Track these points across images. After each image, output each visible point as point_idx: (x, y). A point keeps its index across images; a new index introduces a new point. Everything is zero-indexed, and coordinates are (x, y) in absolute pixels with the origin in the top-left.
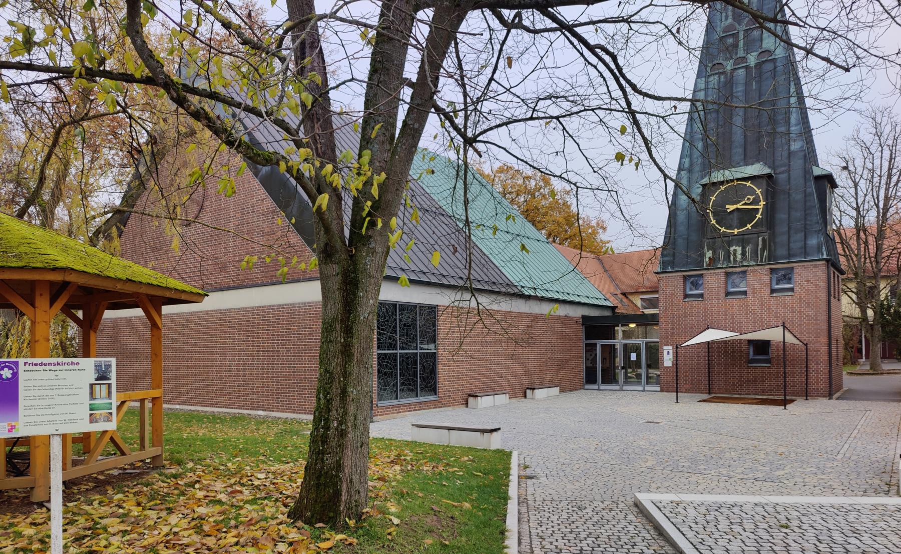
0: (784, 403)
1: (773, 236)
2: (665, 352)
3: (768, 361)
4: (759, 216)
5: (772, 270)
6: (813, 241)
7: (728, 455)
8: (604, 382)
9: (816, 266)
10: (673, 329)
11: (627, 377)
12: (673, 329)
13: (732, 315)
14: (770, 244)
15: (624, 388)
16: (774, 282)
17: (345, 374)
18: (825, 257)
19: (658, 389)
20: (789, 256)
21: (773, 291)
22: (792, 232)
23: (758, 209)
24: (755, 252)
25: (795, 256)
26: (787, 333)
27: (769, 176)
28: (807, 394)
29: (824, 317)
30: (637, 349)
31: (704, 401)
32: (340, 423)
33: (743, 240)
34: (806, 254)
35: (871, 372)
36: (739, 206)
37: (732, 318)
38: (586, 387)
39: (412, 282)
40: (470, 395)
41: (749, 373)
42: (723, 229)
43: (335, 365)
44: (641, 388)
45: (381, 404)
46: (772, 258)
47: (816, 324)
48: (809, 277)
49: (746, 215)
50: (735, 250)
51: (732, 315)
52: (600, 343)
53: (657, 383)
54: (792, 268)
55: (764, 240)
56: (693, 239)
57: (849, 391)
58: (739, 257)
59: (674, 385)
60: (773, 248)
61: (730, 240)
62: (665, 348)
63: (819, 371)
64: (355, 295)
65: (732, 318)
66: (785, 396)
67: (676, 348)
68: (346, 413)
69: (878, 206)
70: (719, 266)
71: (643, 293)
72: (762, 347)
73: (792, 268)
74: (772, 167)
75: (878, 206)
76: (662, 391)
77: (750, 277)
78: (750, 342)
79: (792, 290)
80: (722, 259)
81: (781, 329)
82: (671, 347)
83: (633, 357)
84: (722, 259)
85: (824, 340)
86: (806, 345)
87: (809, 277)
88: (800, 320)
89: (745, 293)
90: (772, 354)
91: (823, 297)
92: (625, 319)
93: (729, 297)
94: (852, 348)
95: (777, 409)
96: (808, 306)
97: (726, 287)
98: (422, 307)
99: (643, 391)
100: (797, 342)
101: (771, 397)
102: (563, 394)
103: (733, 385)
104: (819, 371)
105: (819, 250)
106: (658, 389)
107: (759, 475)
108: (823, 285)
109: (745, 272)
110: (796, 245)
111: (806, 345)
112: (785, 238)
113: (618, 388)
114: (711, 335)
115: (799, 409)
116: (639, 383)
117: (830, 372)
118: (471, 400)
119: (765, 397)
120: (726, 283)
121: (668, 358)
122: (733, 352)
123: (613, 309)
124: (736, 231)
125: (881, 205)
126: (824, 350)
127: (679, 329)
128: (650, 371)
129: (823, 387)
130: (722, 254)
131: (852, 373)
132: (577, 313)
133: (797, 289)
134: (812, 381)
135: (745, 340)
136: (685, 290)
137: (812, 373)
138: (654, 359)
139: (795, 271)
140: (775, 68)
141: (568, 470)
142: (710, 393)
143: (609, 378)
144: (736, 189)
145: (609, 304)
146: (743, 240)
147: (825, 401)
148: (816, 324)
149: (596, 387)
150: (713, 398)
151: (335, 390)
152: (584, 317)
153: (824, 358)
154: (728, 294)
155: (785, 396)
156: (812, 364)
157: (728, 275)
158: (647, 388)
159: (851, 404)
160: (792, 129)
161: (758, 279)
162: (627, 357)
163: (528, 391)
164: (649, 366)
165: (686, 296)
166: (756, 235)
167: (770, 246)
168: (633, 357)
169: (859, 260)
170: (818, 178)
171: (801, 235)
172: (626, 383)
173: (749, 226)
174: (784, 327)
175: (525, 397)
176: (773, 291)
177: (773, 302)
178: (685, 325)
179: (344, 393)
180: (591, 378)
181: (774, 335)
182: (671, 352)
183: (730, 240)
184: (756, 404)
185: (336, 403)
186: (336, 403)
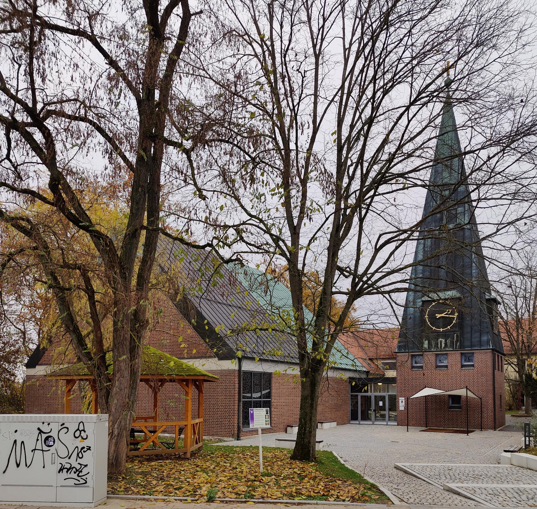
0: (467, 432)
1: (462, 334)
2: (400, 401)
3: (460, 408)
4: (454, 322)
5: (462, 353)
6: (484, 338)
7: (433, 454)
8: (363, 419)
9: (486, 353)
10: (405, 387)
11: (376, 417)
12: (405, 387)
13: (440, 380)
14: (461, 339)
15: (375, 423)
16: (463, 361)
17: (311, 413)
18: (491, 347)
19: (396, 424)
20: (472, 346)
21: (463, 366)
22: (473, 332)
23: (454, 318)
24: (452, 342)
25: (475, 346)
26: (468, 391)
27: (459, 299)
28: (481, 427)
29: (491, 383)
30: (383, 398)
31: (423, 431)
32: (309, 429)
33: (445, 335)
34: (481, 345)
35: (526, 415)
36: (443, 315)
37: (440, 382)
38: (351, 422)
39: (260, 360)
40: (288, 426)
41: (448, 415)
42: (434, 328)
43: (308, 410)
44: (385, 423)
45: (244, 430)
46: (462, 347)
47: (487, 386)
48: (482, 359)
49: (447, 321)
50: (441, 342)
51: (440, 380)
52: (360, 395)
53: (395, 420)
54: (473, 353)
55: (457, 336)
56: (415, 334)
57: (509, 426)
58: (443, 345)
59: (406, 421)
60: (462, 341)
61: (439, 335)
62: (400, 398)
63: (488, 414)
64: (315, 388)
65: (440, 382)
66: (468, 428)
67: (407, 400)
68: (311, 425)
69: (529, 311)
70: (433, 350)
71: (383, 359)
72: (456, 399)
73: (473, 353)
74: (462, 292)
75: (529, 311)
76: (398, 425)
77: (450, 357)
78: (450, 396)
79: (473, 366)
80: (433, 346)
81: (465, 389)
82: (403, 398)
83: (381, 404)
84: (433, 346)
85: (491, 396)
86: (481, 399)
87: (482, 359)
88: (478, 384)
89: (446, 366)
90: (463, 403)
91: (490, 371)
92: (375, 380)
93: (438, 369)
94: (517, 399)
95: (464, 436)
96: (482, 376)
97: (436, 363)
98: (265, 374)
99: (387, 425)
100: (474, 396)
101: (462, 429)
102: (339, 427)
103: (440, 421)
104: (488, 414)
105: (488, 344)
106: (396, 424)
107: (446, 460)
108: (490, 364)
109: (447, 354)
110: (475, 340)
111: (481, 399)
112: (469, 335)
113: (371, 423)
114: (427, 392)
115: (476, 436)
116: (384, 420)
117: (495, 414)
118: (289, 429)
119: (458, 429)
120: (436, 360)
121: (402, 405)
122: (440, 402)
123: (367, 373)
124: (441, 330)
125: (531, 311)
126: (491, 401)
127: (408, 387)
128: (390, 413)
129: (491, 423)
130: (433, 343)
131: (514, 416)
132: (346, 376)
133: (476, 365)
134: (485, 420)
135: (447, 395)
136: (412, 364)
137: (485, 415)
138: (393, 406)
139: (475, 355)
140: (464, 234)
141: (361, 459)
142: (426, 427)
143: (366, 417)
144: (443, 304)
145: (365, 369)
146: (445, 335)
147: (491, 431)
148: (487, 386)
149: (358, 422)
150: (429, 429)
151: (308, 418)
152: (350, 378)
153: (491, 407)
154: (437, 367)
155: (468, 428)
156: (484, 410)
157: (437, 355)
158: (389, 423)
159: (509, 433)
160: (474, 271)
161: (454, 359)
162: (377, 403)
163: (319, 424)
164: (390, 410)
165: (413, 367)
166: (453, 333)
167: (460, 340)
168: (381, 404)
169: (518, 344)
170: (488, 300)
171: (478, 334)
172: (376, 420)
173: (449, 327)
174: (467, 389)
175: (286, 432)
176: (463, 366)
177: (463, 372)
178: (412, 385)
179: (311, 419)
180: (354, 417)
181: (462, 392)
182: (404, 401)
183: (439, 335)
184: (453, 432)
185: (308, 422)
186: (308, 422)
